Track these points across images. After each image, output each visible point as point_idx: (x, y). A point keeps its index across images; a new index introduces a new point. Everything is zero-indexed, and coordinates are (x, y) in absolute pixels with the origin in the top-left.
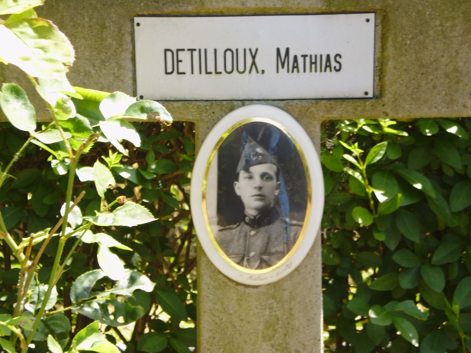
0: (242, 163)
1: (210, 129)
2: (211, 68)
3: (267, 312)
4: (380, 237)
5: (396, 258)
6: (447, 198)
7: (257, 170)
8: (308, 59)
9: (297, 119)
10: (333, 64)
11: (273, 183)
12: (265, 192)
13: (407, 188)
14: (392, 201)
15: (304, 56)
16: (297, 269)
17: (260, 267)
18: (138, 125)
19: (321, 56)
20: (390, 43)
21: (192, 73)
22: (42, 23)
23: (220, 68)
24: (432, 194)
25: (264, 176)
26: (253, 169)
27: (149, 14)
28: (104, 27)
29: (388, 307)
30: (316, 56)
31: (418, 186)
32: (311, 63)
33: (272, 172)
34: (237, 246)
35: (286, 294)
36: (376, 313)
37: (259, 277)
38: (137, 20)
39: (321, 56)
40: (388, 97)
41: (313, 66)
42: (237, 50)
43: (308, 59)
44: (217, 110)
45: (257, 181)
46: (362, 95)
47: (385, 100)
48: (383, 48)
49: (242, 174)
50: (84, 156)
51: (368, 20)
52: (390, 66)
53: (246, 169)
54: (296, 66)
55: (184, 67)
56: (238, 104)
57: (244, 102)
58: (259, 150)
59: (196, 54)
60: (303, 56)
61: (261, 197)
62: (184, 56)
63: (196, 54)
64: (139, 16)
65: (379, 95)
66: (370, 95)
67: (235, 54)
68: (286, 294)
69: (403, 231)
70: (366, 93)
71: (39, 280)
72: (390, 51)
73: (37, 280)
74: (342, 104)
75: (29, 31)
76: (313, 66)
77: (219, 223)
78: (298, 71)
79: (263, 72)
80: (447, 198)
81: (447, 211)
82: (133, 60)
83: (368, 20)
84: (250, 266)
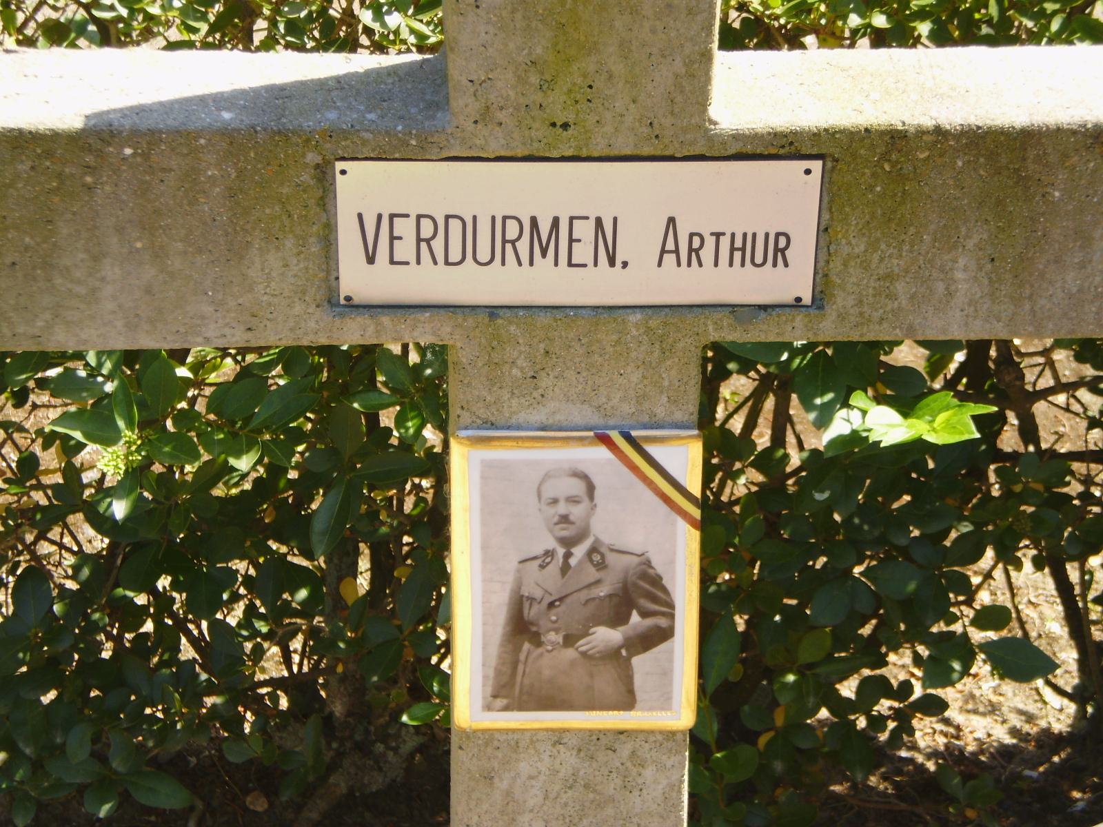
8: (725, 243)
15: (718, 235)
19: (754, 235)
21: (716, 264)
27: (563, 156)
30: (745, 235)
32: (733, 249)
38: (340, 165)
39: (754, 235)
41: (738, 255)
42: (475, 218)
43: (725, 243)
46: (788, 298)
50: (905, 410)
51: (808, 172)
55: (583, 253)
56: (842, 317)
60: (712, 234)
64: (343, 159)
66: (807, 299)
67: (470, 227)
70: (798, 299)
71: (12, 598)
73: (9, 596)
74: (779, 316)
76: (738, 255)
78: (700, 265)
79: (625, 264)
83: (808, 172)
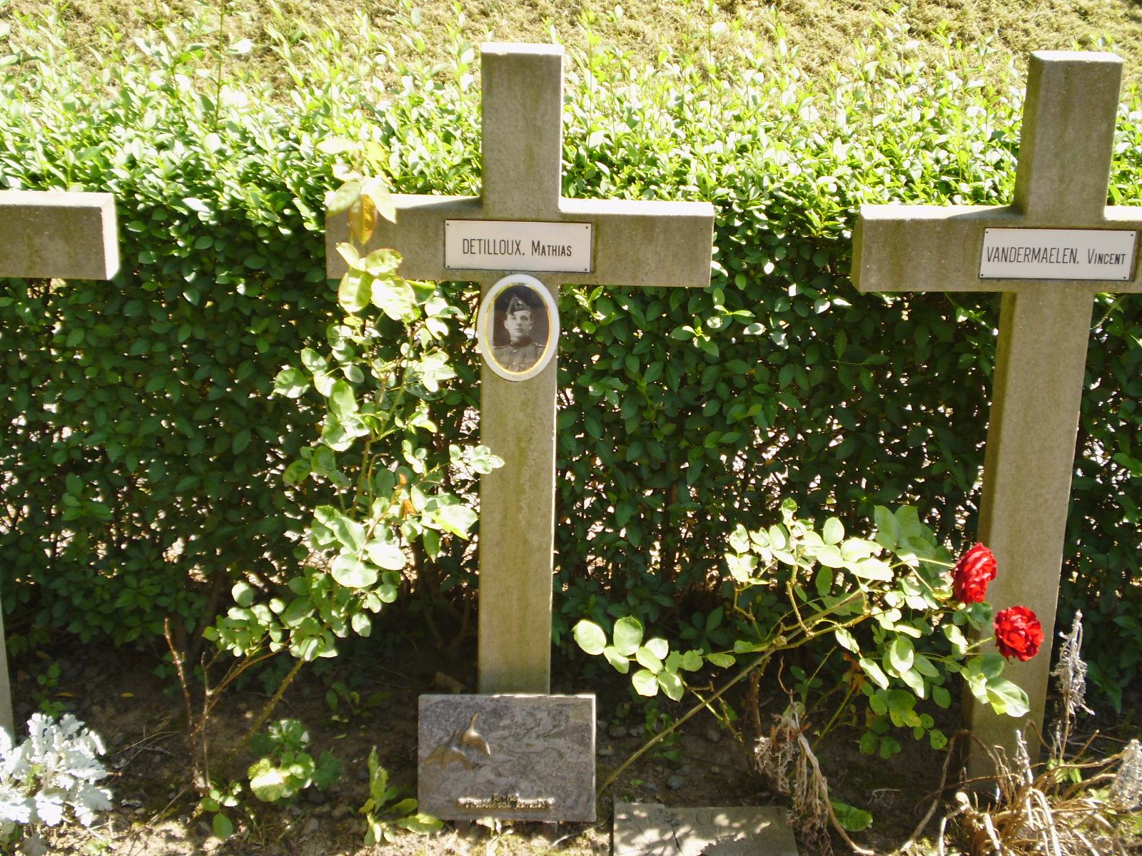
0: (509, 310)
1: (490, 287)
2: (492, 251)
3: (523, 396)
4: (600, 339)
5: (610, 351)
6: (644, 311)
7: (519, 314)
9: (544, 284)
10: (566, 251)
11: (529, 322)
12: (524, 327)
13: (618, 308)
14: (609, 317)
16: (542, 372)
17: (519, 371)
18: (446, 321)
20: (600, 242)
22: (397, 279)
23: (497, 251)
24: (634, 312)
25: (523, 318)
26: (515, 313)
28: (427, 226)
29: (602, 381)
31: (625, 308)
33: (528, 316)
34: (506, 358)
35: (534, 386)
36: (594, 388)
37: (518, 377)
38: (447, 222)
40: (598, 273)
44: (495, 276)
45: (519, 321)
47: (597, 274)
48: (596, 243)
49: (509, 316)
52: (600, 254)
53: (512, 312)
54: (544, 251)
55: (476, 249)
57: (512, 272)
58: (520, 302)
59: (482, 242)
61: (521, 330)
62: (476, 244)
63: (482, 242)
65: (593, 271)
67: (506, 243)
68: (534, 386)
69: (615, 334)
72: (600, 247)
75: (391, 282)
77: (495, 345)
80: (644, 311)
81: (644, 321)
82: (444, 244)
84: (513, 369)
